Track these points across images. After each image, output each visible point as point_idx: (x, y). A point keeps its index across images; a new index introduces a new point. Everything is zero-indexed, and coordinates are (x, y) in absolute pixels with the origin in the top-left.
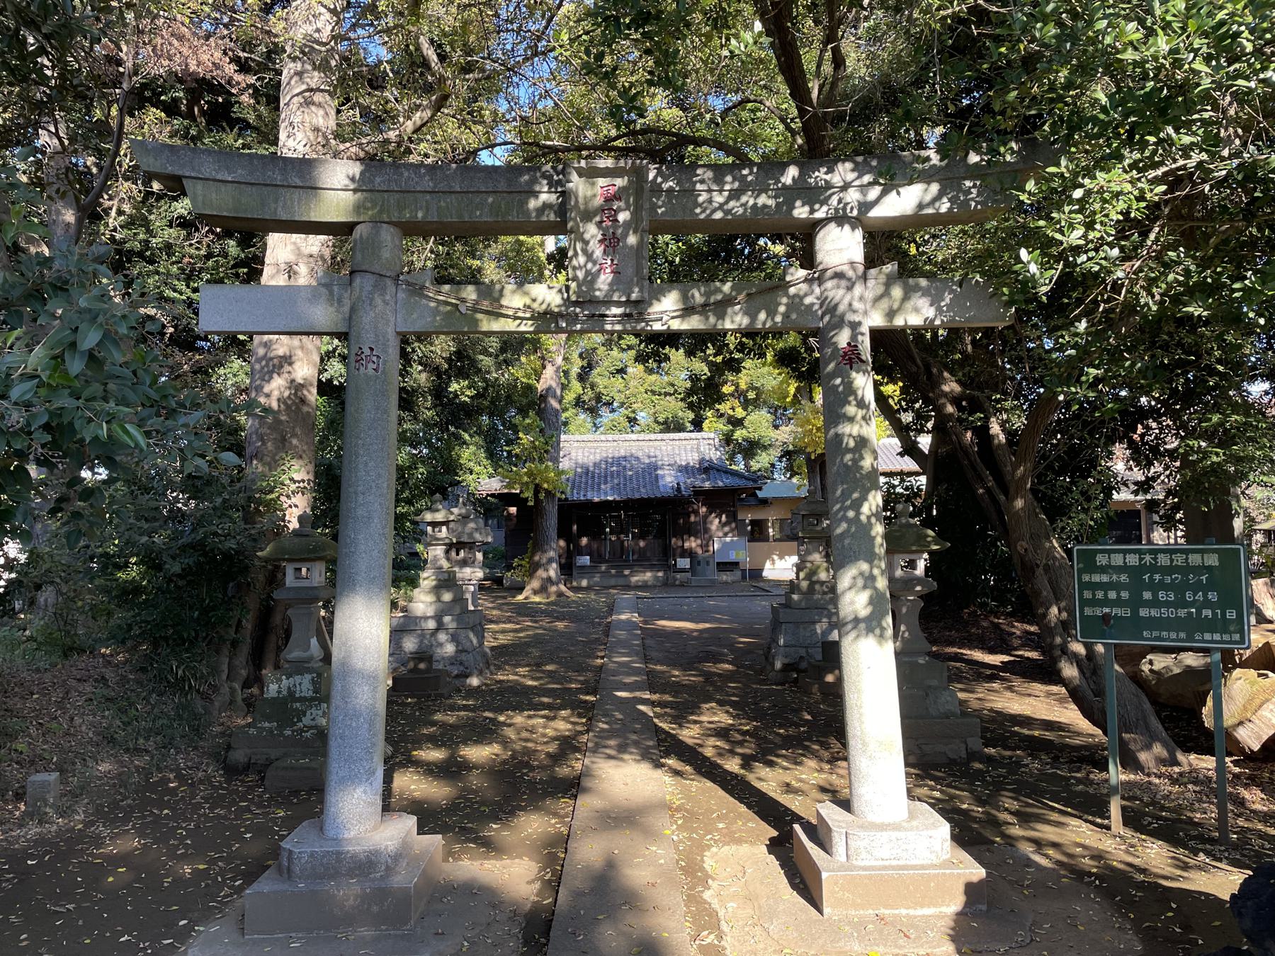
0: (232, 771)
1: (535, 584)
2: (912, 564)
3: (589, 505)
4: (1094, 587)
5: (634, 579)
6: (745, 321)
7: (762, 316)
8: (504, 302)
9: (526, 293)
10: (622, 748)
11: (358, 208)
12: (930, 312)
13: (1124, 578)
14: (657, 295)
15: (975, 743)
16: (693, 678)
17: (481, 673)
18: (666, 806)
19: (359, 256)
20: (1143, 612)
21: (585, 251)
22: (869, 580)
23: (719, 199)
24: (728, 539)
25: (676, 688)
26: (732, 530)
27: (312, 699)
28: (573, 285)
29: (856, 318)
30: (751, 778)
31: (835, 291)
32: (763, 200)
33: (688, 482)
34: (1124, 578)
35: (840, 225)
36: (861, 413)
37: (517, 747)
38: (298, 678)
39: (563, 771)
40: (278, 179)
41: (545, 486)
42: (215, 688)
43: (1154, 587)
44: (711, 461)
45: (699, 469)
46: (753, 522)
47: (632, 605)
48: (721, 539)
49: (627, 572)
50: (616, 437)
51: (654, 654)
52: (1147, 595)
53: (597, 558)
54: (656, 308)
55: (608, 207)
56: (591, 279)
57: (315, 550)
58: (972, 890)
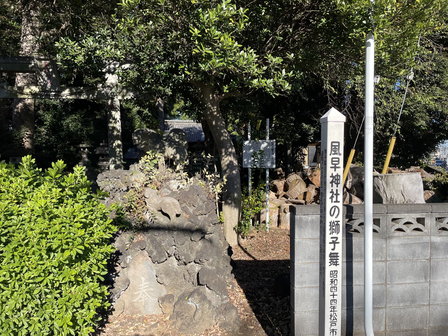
7: (91, 96)
8: (24, 91)
9: (30, 88)
14: (64, 89)
21: (42, 79)
35: (109, 73)
36: (113, 121)
56: (45, 85)
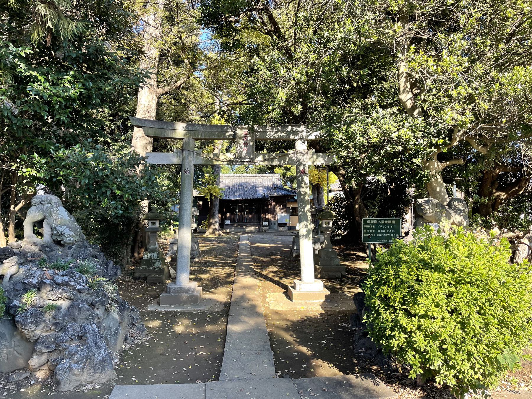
0: (135, 279)
1: (210, 230)
2: (329, 223)
3: (230, 201)
4: (367, 229)
5: (247, 230)
6: (278, 163)
7: (282, 162)
10: (246, 275)
11: (185, 135)
12: (323, 162)
13: (373, 226)
15: (344, 273)
16: (267, 260)
17: (198, 258)
18: (256, 285)
19: (185, 146)
20: (378, 235)
22: (306, 226)
23: (272, 134)
24: (283, 215)
25: (262, 262)
26: (284, 211)
27: (157, 259)
28: (237, 154)
29: (304, 163)
30: (281, 281)
31: (300, 156)
32: (283, 134)
33: (268, 193)
34: (373, 226)
37: (215, 275)
38: (153, 254)
39: (229, 280)
40: (165, 127)
41: (214, 194)
42: (123, 258)
43: (380, 229)
44: (277, 185)
45: (272, 188)
46: (292, 208)
47: (246, 238)
48: (280, 215)
49: (244, 227)
50: (241, 175)
51: (254, 253)
52: (379, 231)
53: (233, 221)
54: (257, 160)
55: (245, 136)
57: (158, 217)
58: (327, 296)
